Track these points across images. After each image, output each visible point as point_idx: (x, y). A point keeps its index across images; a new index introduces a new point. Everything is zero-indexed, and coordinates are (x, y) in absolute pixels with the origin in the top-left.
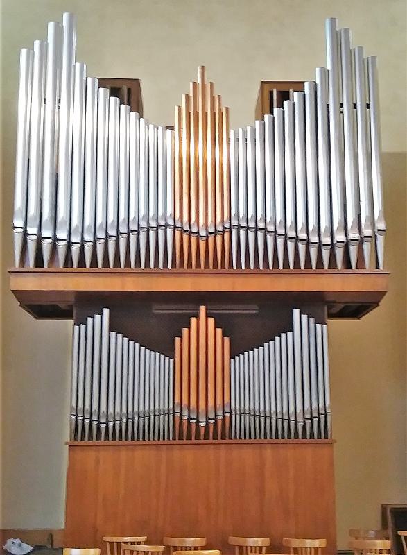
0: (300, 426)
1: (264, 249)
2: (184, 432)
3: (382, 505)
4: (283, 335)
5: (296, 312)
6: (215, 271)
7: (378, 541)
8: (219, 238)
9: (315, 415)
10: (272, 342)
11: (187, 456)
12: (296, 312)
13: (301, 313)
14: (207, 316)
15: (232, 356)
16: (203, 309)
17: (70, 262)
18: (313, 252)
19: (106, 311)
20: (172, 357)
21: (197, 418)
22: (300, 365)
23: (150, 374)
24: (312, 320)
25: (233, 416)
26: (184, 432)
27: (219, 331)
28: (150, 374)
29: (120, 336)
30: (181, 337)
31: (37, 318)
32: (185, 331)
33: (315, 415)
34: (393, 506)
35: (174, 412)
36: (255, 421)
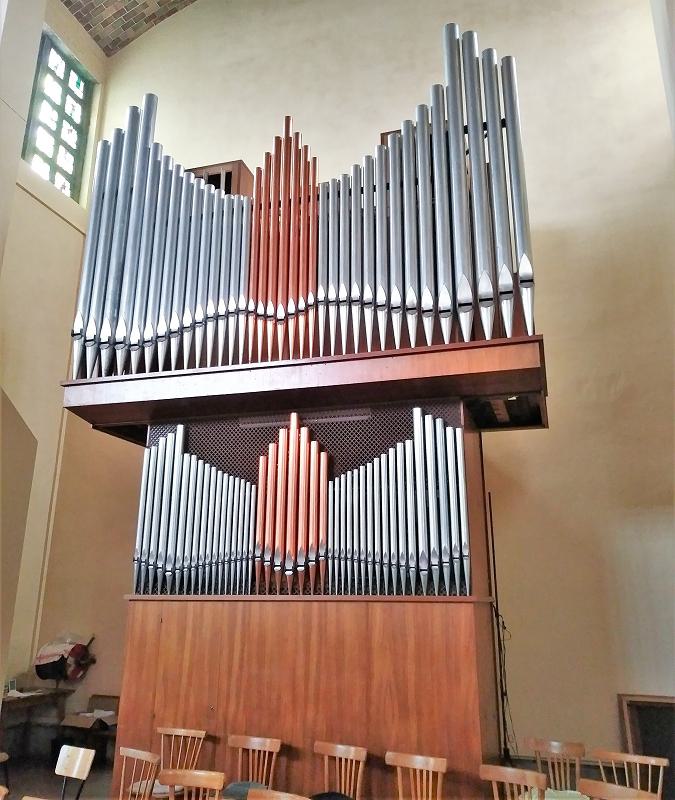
0: (424, 575)
1: (388, 326)
2: (262, 580)
3: (619, 695)
4: (399, 445)
5: (417, 412)
6: (339, 357)
7: (340, 747)
8: (302, 319)
9: (446, 559)
10: (383, 456)
11: (267, 610)
12: (417, 412)
13: (424, 414)
14: (299, 426)
15: (331, 477)
16: (294, 416)
17: (457, 330)
18: (428, 323)
19: (180, 428)
20: (255, 482)
21: (272, 560)
22: (263, 499)
23: (437, 488)
24: (439, 422)
25: (330, 562)
26: (262, 580)
27: (314, 444)
28: (437, 488)
29: (194, 457)
30: (413, 438)
31: (36, 442)
32: (272, 446)
33: (446, 559)
34: (630, 699)
35: (254, 557)
36: (224, 570)
